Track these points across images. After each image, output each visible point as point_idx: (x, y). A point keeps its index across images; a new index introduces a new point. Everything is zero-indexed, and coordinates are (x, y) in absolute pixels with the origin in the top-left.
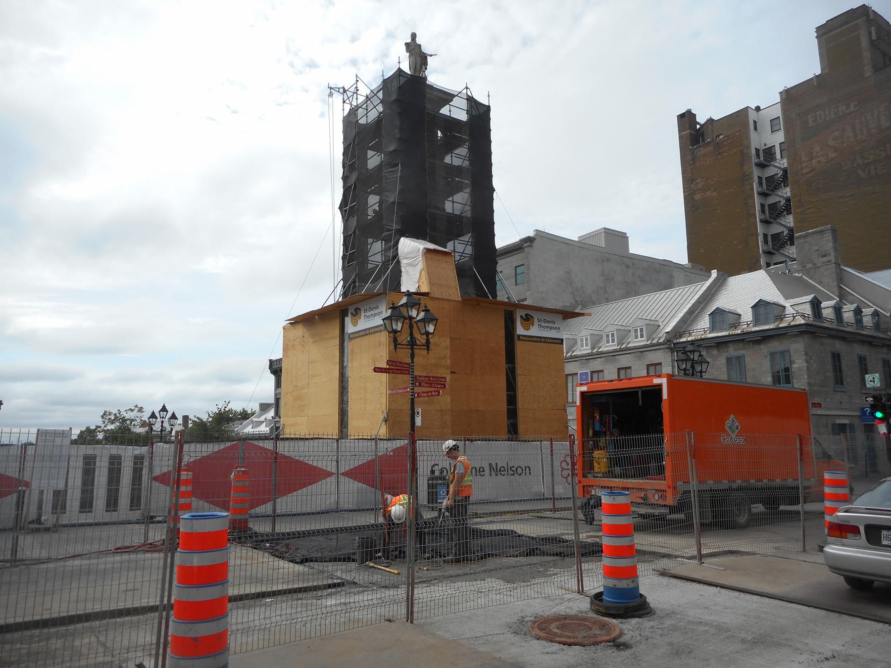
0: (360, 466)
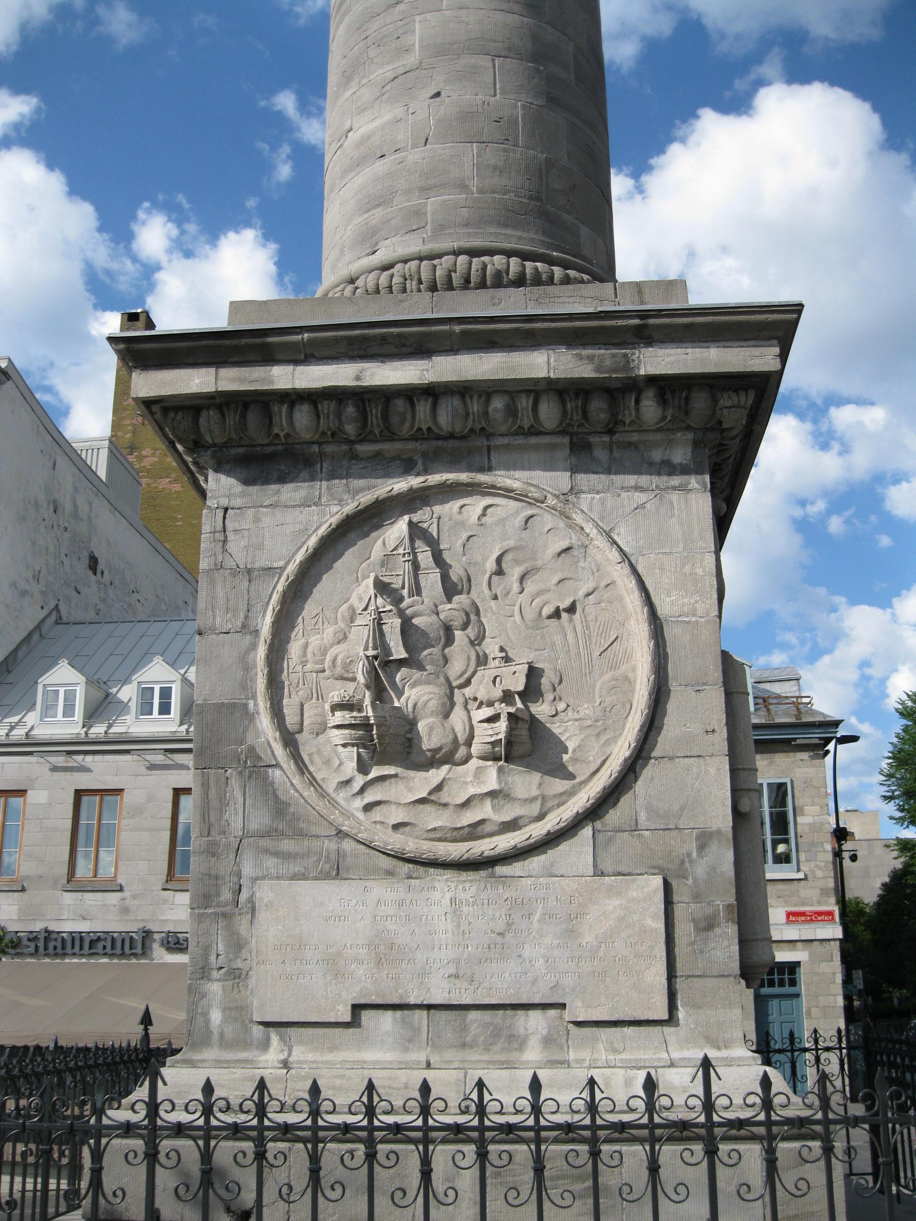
0: (377, 530)
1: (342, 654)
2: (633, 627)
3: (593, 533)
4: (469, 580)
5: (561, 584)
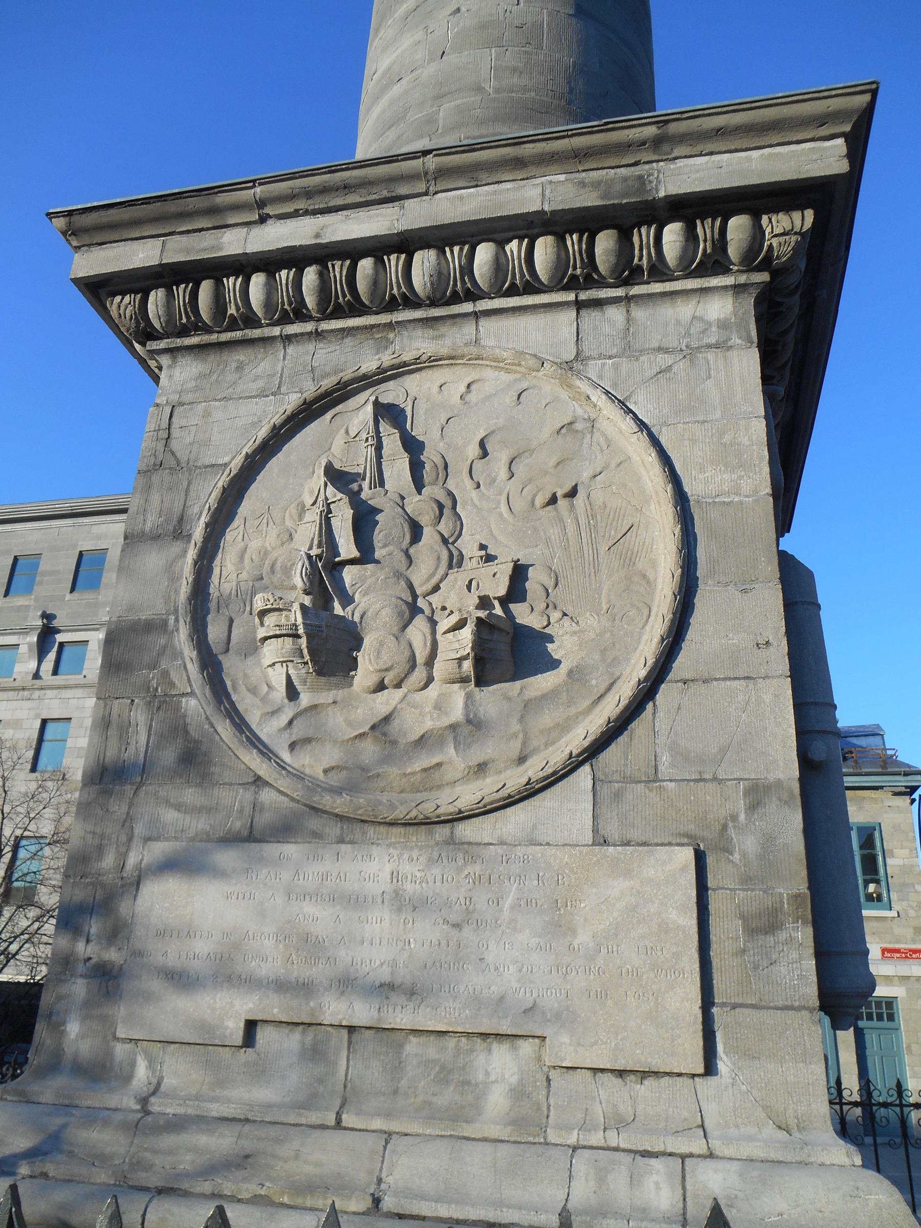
1: (283, 557)
2: (654, 512)
3: (598, 397)
4: (446, 467)
5: (560, 466)
